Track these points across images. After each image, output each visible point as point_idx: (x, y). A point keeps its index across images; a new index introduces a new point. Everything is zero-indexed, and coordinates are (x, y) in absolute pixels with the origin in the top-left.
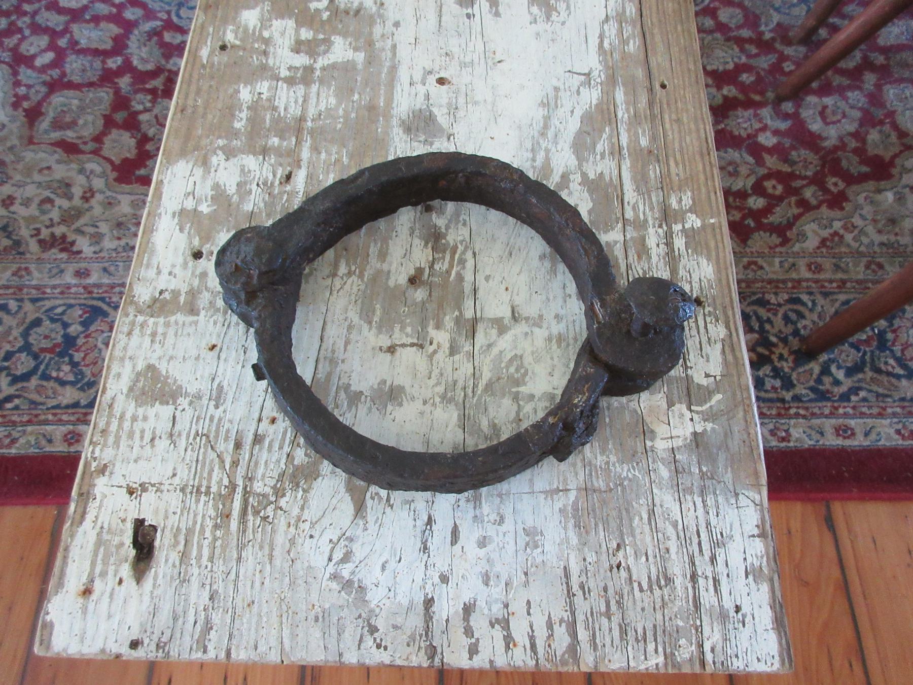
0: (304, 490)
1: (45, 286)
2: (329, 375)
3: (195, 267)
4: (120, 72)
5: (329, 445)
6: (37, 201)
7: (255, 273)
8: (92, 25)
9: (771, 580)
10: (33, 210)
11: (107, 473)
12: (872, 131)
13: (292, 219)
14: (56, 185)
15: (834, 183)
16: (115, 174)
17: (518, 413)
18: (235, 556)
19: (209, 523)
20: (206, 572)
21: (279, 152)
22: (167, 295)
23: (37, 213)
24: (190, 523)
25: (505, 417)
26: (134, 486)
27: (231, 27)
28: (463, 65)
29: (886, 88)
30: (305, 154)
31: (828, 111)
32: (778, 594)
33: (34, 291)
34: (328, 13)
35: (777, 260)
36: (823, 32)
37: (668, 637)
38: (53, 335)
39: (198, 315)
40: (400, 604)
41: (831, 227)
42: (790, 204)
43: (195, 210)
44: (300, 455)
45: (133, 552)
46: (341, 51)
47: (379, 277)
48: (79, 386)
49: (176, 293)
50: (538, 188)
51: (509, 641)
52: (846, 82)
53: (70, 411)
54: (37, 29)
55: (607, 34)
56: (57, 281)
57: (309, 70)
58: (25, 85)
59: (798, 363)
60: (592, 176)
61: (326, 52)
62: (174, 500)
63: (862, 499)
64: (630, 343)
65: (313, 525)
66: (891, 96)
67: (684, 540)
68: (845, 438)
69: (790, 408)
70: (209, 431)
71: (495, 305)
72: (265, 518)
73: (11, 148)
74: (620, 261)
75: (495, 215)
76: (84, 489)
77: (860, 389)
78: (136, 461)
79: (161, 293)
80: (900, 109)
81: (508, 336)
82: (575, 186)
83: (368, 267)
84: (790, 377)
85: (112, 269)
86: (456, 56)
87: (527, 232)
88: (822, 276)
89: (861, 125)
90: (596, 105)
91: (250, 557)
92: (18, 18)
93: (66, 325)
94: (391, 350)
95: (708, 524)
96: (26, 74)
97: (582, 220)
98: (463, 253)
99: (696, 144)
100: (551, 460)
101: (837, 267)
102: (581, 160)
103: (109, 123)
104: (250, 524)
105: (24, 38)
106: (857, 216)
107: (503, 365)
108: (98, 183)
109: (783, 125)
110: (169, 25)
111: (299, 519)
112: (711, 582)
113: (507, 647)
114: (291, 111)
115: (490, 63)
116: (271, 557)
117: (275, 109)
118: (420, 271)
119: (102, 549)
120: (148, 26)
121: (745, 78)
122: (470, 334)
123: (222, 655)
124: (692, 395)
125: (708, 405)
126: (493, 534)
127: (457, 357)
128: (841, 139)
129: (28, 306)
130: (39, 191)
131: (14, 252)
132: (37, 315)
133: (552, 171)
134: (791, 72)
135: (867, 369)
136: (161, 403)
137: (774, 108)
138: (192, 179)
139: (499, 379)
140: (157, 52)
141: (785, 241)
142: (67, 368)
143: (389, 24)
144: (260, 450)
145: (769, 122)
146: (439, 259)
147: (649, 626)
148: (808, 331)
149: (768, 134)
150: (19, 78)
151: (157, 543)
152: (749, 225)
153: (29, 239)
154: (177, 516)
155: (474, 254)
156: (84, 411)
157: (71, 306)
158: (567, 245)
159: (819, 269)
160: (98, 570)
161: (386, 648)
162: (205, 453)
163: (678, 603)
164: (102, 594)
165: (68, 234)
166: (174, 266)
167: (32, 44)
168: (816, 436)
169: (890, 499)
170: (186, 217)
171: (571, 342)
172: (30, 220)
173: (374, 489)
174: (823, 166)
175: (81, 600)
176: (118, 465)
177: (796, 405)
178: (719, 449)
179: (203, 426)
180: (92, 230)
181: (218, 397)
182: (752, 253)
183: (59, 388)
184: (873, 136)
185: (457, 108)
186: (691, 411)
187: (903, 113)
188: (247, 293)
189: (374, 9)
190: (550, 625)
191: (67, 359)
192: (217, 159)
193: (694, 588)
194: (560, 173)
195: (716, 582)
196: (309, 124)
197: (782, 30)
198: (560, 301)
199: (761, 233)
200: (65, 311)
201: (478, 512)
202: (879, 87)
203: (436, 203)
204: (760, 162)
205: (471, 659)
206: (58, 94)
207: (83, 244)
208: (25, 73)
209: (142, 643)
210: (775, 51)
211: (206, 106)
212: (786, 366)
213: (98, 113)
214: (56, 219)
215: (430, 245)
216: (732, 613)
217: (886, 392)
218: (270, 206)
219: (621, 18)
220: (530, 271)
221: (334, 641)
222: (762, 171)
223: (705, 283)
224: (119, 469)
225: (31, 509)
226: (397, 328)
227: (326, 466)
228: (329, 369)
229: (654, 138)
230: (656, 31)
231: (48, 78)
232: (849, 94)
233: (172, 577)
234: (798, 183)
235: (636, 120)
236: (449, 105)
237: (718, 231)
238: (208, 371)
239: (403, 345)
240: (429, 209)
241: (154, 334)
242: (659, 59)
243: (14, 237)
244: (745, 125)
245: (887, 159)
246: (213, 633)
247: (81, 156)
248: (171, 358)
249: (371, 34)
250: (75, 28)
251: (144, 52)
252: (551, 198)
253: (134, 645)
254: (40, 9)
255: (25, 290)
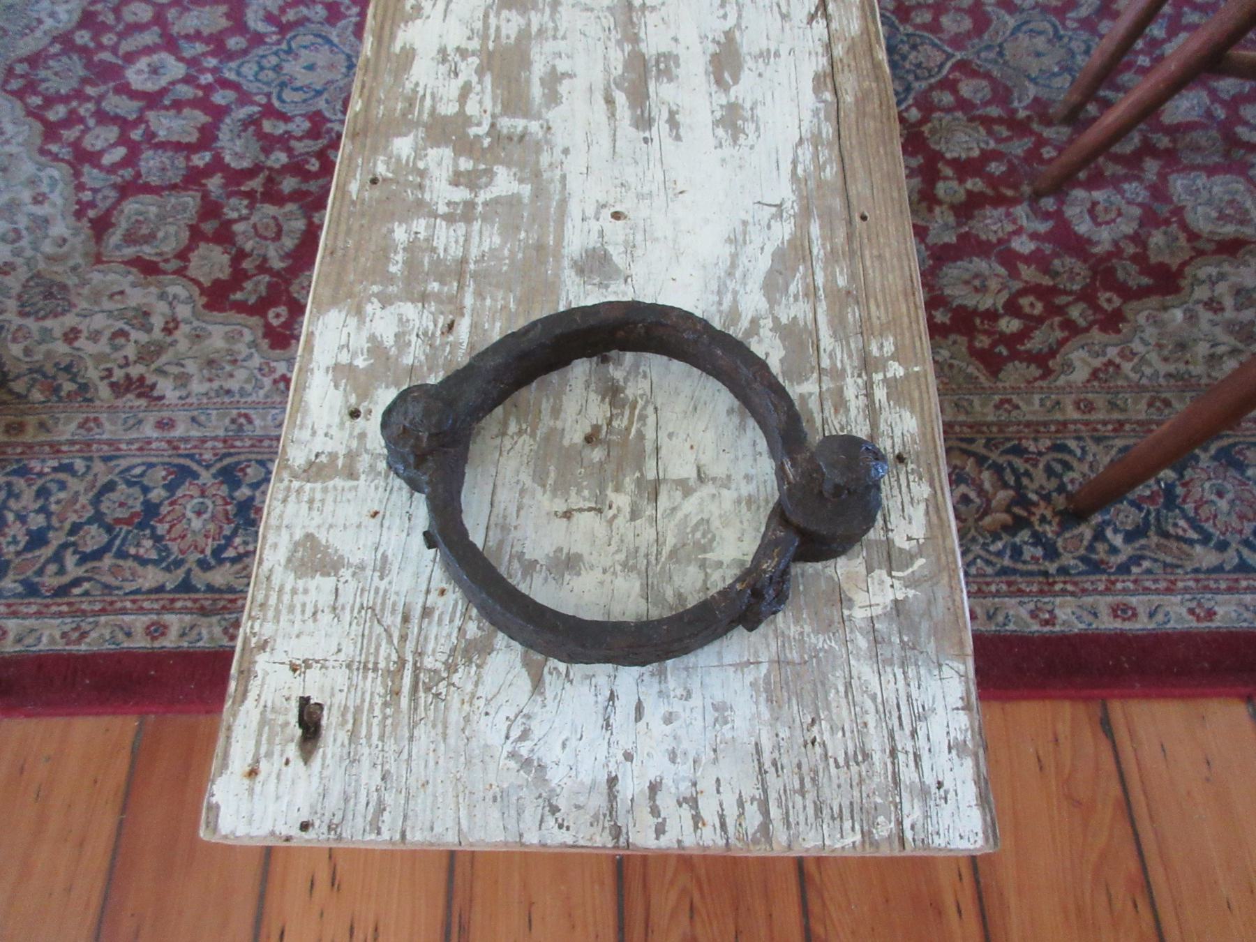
0: (478, 666)
1: (120, 441)
2: (501, 544)
3: (353, 428)
4: (208, 171)
5: (508, 615)
6: (107, 334)
7: (425, 435)
8: (172, 112)
9: (976, 755)
10: (103, 346)
11: (268, 649)
12: (1154, 232)
13: (458, 378)
14: (131, 314)
15: (1108, 300)
16: (204, 300)
17: (705, 582)
18: (407, 735)
19: (378, 701)
20: (376, 751)
21: (438, 297)
22: (323, 459)
23: (108, 350)
24: (358, 701)
25: (691, 585)
26: (298, 662)
27: (382, 158)
28: (640, 197)
29: (1172, 177)
30: (469, 300)
31: (1100, 208)
32: (983, 769)
33: (105, 448)
34: (489, 140)
35: (1036, 398)
36: (1092, 108)
37: (865, 813)
38: (130, 502)
39: (357, 479)
40: (582, 783)
41: (1104, 354)
42: (1051, 327)
43: (351, 364)
44: (472, 629)
45: (299, 732)
46: (504, 183)
47: (553, 437)
48: (164, 565)
49: (333, 456)
50: (723, 339)
51: (697, 820)
52: (1120, 170)
53: (153, 596)
54: (103, 117)
55: (801, 159)
56: (134, 435)
57: (470, 205)
58: (91, 189)
59: (1064, 527)
60: (784, 320)
61: (487, 185)
62: (340, 677)
63: (1147, 696)
64: (824, 506)
65: (488, 702)
66: (1179, 189)
67: (883, 714)
68: (1124, 620)
69: (1055, 582)
70: (374, 603)
71: (679, 466)
72: (437, 695)
73: (74, 269)
74: (815, 415)
75: (677, 366)
76: (245, 666)
77: (1143, 557)
78: (298, 636)
79: (317, 455)
80: (1189, 205)
81: (694, 499)
82: (765, 332)
83: (541, 425)
84: (1055, 543)
85: (203, 418)
86: (633, 187)
87: (713, 384)
88: (1094, 416)
89: (1141, 225)
90: (789, 241)
91: (423, 737)
92: (80, 105)
93: (146, 490)
94: (567, 515)
95: (909, 696)
96: (91, 175)
97: (770, 373)
98: (644, 408)
99: (899, 282)
100: (739, 634)
101: (1113, 405)
102: (772, 302)
103: (196, 235)
104: (422, 701)
105: (87, 130)
106: (1137, 340)
107: (689, 530)
108: (183, 311)
109: (1043, 227)
110: (269, 111)
111: (473, 696)
112: (911, 756)
113: (696, 827)
114: (451, 251)
115: (671, 195)
116: (445, 736)
117: (434, 250)
118: (596, 428)
119: (266, 728)
120: (243, 112)
121: (996, 168)
122: (653, 497)
123: (397, 837)
124: (891, 559)
125: (910, 570)
126: (681, 710)
127: (638, 522)
128: (1116, 243)
129: (99, 467)
130: (110, 322)
131: (80, 399)
132: (110, 477)
133: (740, 315)
134: (1051, 160)
135: (1151, 533)
136: (323, 575)
137: (1030, 206)
138: (345, 331)
139: (684, 545)
140: (255, 146)
141: (1047, 373)
142: (148, 543)
143: (558, 150)
144: (430, 623)
145: (1024, 222)
146: (617, 415)
147: (845, 803)
148: (1077, 486)
149: (1024, 238)
150: (83, 180)
151: (324, 722)
152: (1000, 353)
153: (98, 382)
154: (344, 694)
155: (656, 409)
156: (171, 596)
157: (151, 466)
158: (757, 400)
159: (1090, 407)
160: (263, 750)
161: (568, 828)
162: (371, 627)
163: (876, 779)
164: (269, 775)
165: (147, 375)
166: (329, 426)
167: (98, 137)
168: (1088, 618)
169: (1182, 697)
170: (341, 372)
171: (762, 503)
172: (99, 358)
173: (553, 662)
174: (1093, 279)
175: (246, 781)
176: (279, 640)
177: (1062, 579)
178: (921, 616)
179: (369, 599)
180: (175, 370)
181: (383, 568)
182: (1004, 388)
183: (140, 569)
184: (1157, 238)
185: (634, 246)
186: (892, 577)
187: (1194, 209)
188: (416, 456)
189: (540, 135)
190: (741, 804)
191: (148, 532)
192: (372, 308)
193: (893, 763)
194: (749, 317)
195: (917, 757)
196: (472, 266)
197: (1040, 107)
198: (750, 459)
199: (1017, 363)
200: (144, 472)
201: (663, 686)
202: (1163, 177)
203: (614, 353)
204: (1014, 273)
205: (657, 838)
206: (131, 199)
207: (165, 387)
208: (90, 174)
209: (313, 825)
210: (1032, 133)
211: (357, 249)
212: (1049, 530)
213: (182, 223)
214: (132, 358)
215: (607, 400)
216: (934, 789)
217: (1175, 561)
218: (431, 359)
219: (816, 140)
220: (717, 427)
221: (514, 821)
222: (1017, 285)
223: (908, 438)
224: (281, 645)
225: (105, 721)
226: (573, 491)
227: (501, 639)
228: (499, 537)
229: (852, 277)
230: (856, 155)
231: (119, 180)
232: (1126, 186)
233: (341, 757)
234: (1061, 300)
235: (832, 257)
236: (626, 242)
237: (923, 379)
238: (372, 539)
239: (581, 510)
240: (605, 360)
241: (311, 501)
242: (859, 188)
243: (80, 381)
244: (994, 228)
245: (1174, 268)
246: (386, 814)
247: (161, 277)
248: (331, 526)
249: (538, 162)
250: (151, 115)
251: (239, 145)
252: (738, 349)
253: (305, 827)
254: (107, 92)
255: (95, 447)
